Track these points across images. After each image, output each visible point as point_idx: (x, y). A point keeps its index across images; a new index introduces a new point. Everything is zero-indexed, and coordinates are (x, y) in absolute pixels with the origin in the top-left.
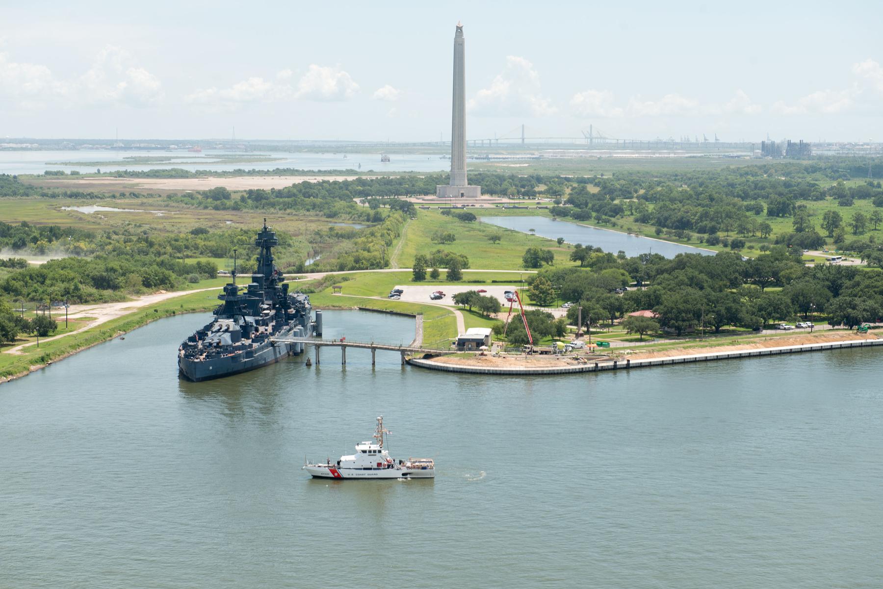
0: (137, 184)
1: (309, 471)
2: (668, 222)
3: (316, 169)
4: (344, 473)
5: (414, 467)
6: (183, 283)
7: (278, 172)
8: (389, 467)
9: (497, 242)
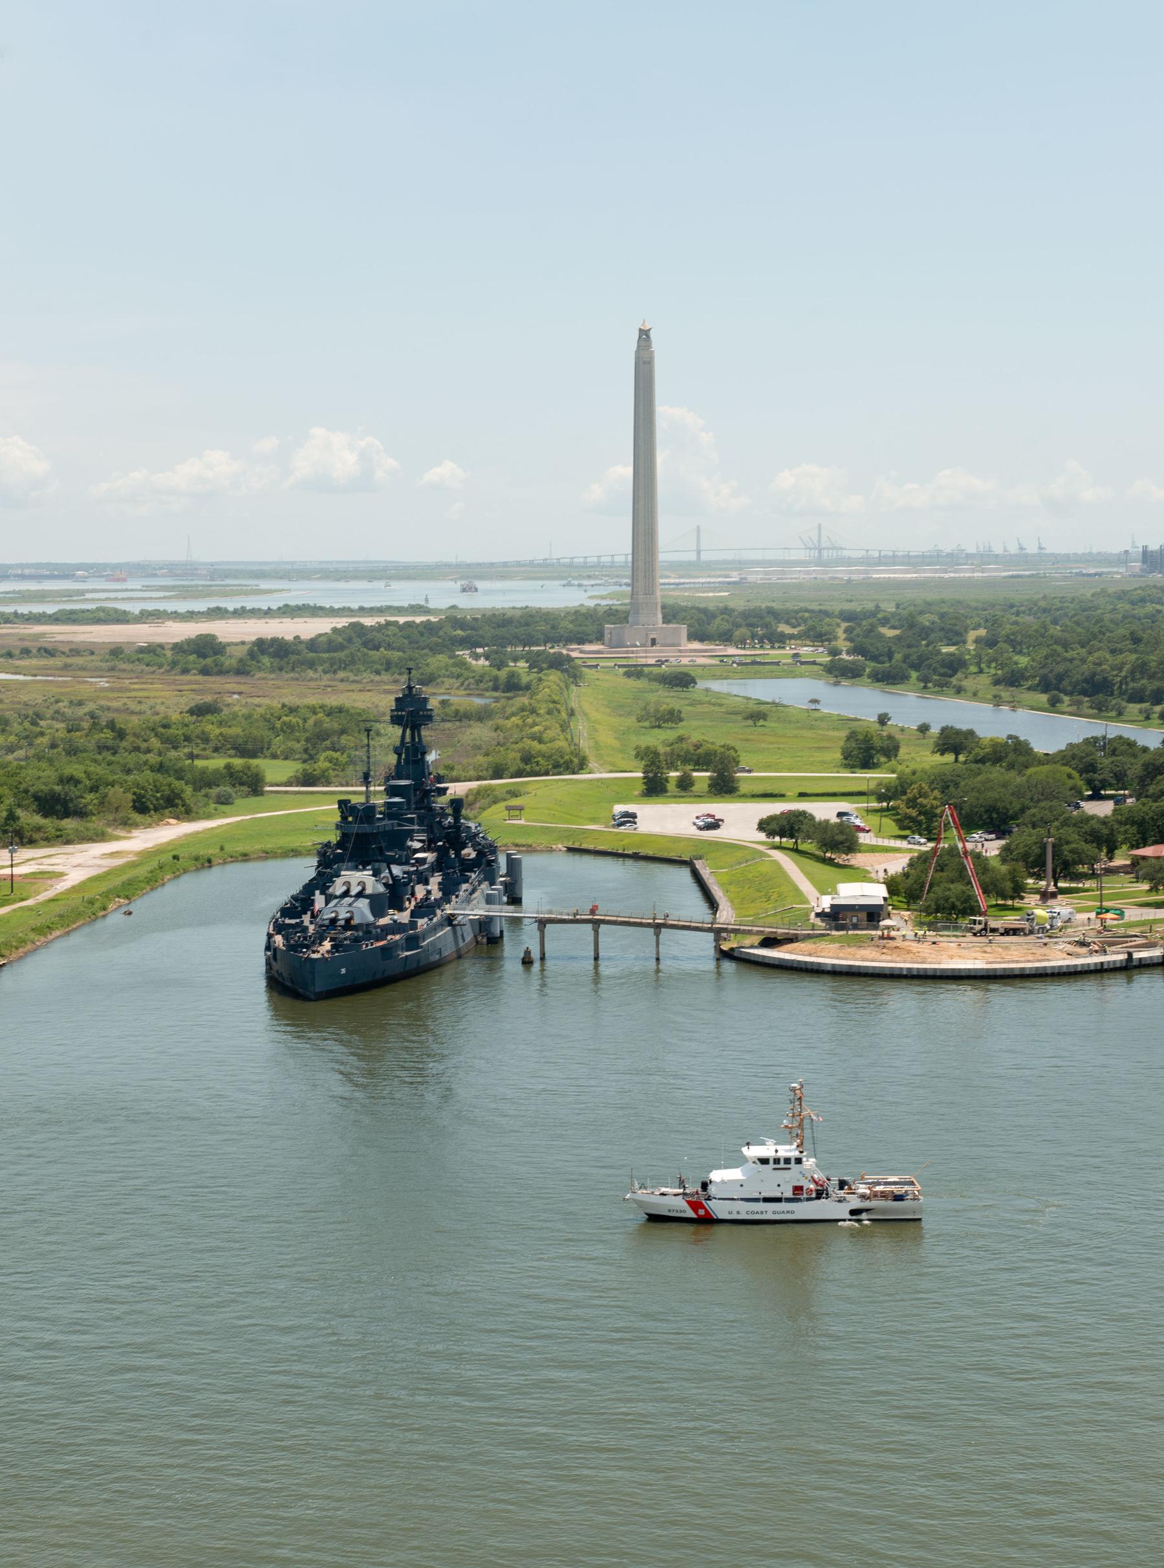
0: (43, 635)
1: (640, 1204)
2: (1065, 683)
3: (355, 606)
4: (719, 1209)
5: (876, 1195)
6: (206, 805)
7: (288, 611)
8: (819, 1195)
9: (761, 722)
